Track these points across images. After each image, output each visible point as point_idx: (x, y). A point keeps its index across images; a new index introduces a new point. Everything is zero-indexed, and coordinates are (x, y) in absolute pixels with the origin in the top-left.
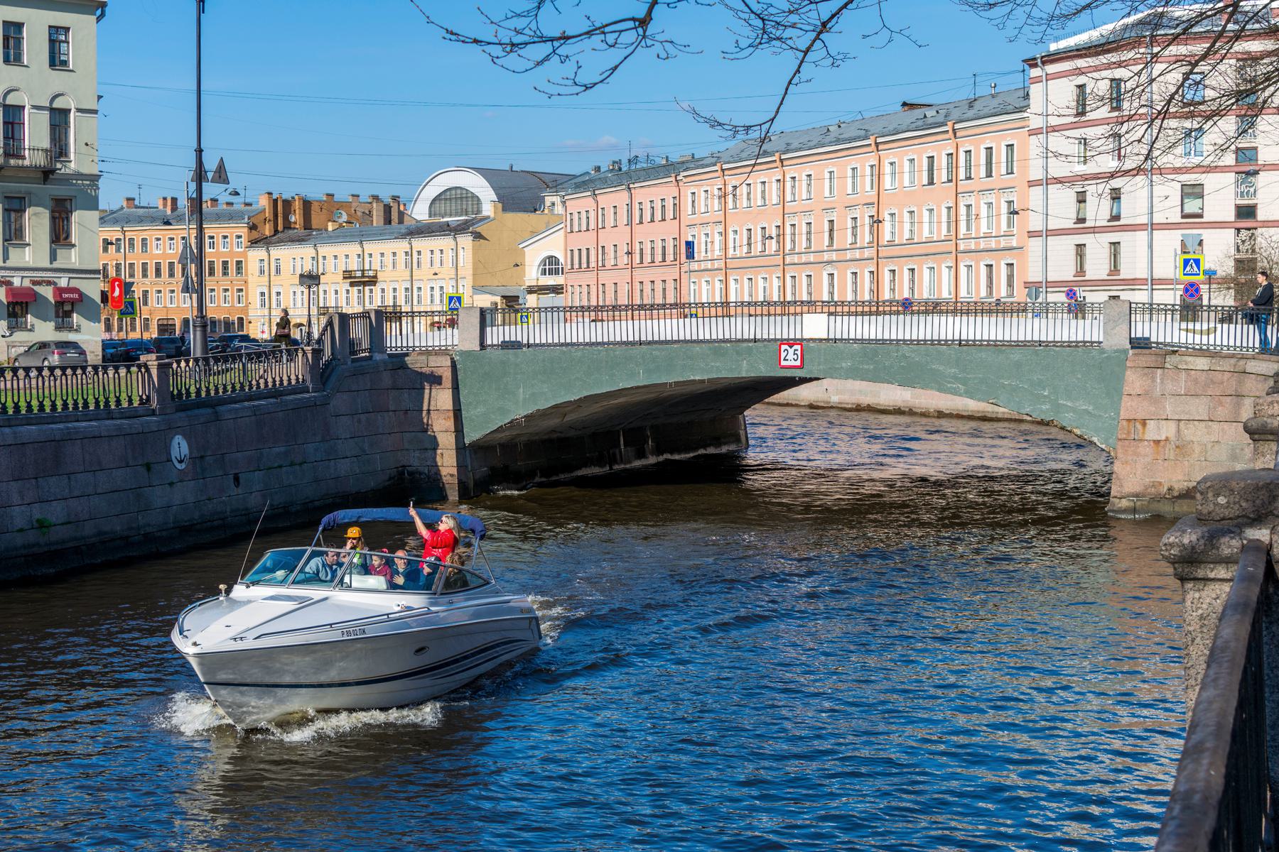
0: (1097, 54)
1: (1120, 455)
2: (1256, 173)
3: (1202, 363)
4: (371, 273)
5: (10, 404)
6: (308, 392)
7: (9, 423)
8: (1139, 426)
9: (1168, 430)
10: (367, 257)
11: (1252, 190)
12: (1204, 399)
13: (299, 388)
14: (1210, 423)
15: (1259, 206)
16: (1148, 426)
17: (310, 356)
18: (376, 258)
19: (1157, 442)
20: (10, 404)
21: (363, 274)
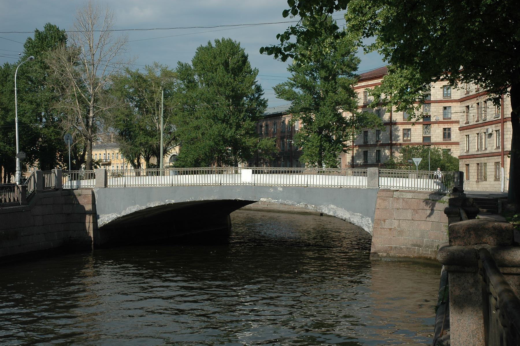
0: (61, 309)
1: (375, 235)
2: (430, 125)
3: (409, 196)
4: (109, 161)
5: (3, 199)
6: (20, 205)
7: (3, 206)
8: (383, 222)
9: (396, 224)
10: (107, 154)
11: (429, 131)
12: (410, 211)
13: (16, 203)
14: (413, 221)
15: (431, 137)
16: (386, 222)
17: (21, 189)
18: (111, 154)
19: (390, 229)
20: (3, 199)
21: (106, 161)
